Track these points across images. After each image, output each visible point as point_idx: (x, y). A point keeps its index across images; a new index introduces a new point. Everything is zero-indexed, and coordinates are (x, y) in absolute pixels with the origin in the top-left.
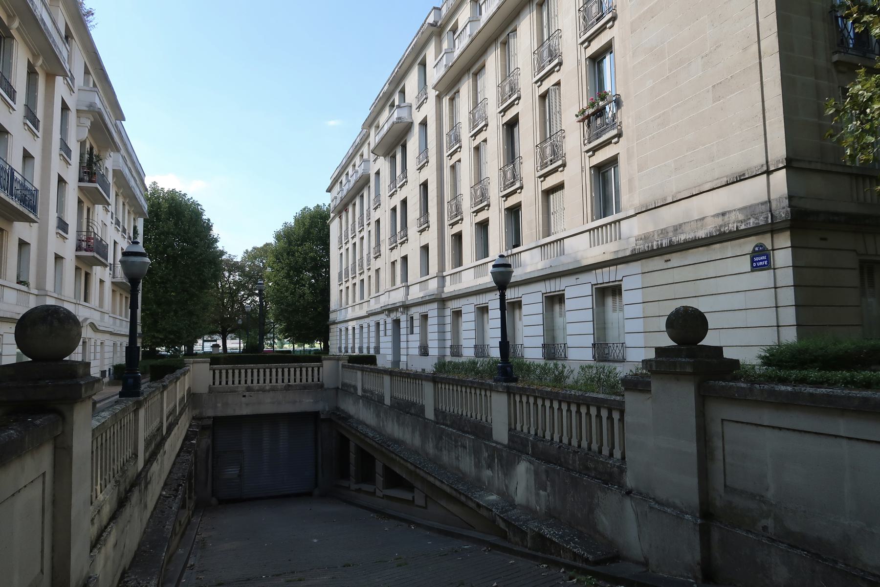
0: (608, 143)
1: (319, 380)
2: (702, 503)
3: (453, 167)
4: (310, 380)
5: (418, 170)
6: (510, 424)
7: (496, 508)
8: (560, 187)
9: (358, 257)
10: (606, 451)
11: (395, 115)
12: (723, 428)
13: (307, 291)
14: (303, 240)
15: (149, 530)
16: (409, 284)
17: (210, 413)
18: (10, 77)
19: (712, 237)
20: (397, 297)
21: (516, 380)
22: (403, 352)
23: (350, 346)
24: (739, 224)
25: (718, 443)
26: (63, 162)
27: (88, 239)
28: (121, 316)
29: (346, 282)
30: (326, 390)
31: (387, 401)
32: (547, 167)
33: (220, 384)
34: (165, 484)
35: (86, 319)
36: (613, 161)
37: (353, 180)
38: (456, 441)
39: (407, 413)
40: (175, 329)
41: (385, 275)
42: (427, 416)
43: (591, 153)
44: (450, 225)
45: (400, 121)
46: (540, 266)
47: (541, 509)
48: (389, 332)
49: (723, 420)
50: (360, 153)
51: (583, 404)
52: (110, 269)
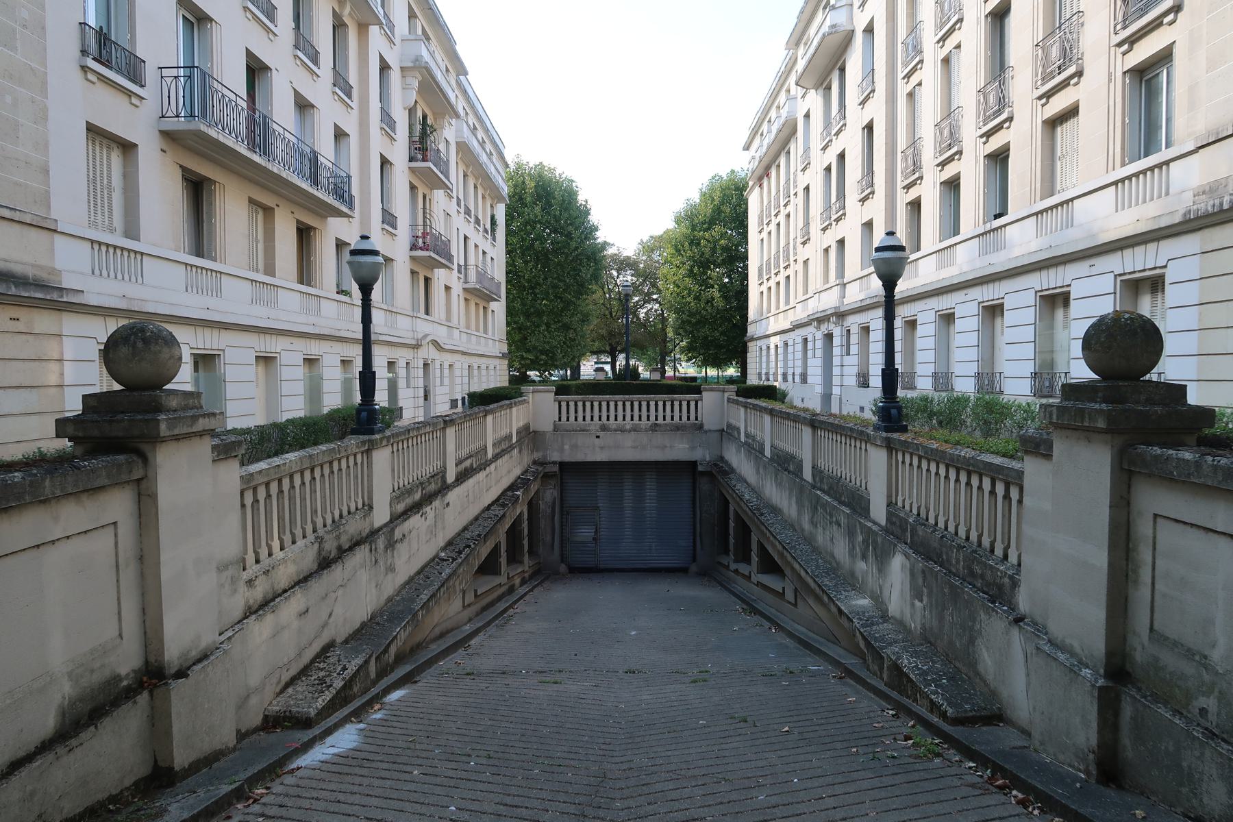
0: (1156, 24)
1: (697, 419)
2: (1110, 654)
3: (911, 95)
4: (684, 418)
5: (860, 104)
6: (889, 496)
7: (860, 619)
8: (1071, 112)
9: (782, 244)
10: (999, 552)
11: (828, 23)
12: (1155, 529)
13: (717, 295)
14: (711, 222)
15: (398, 598)
16: (846, 281)
17: (556, 457)
18: (311, 34)
20: (829, 301)
21: (904, 429)
22: (836, 381)
23: (772, 371)
25: (1145, 555)
26: (385, 137)
27: (425, 235)
28: (479, 332)
29: (768, 280)
30: (706, 432)
31: (768, 453)
32: (1053, 78)
33: (568, 420)
34: (450, 543)
35: (426, 336)
36: (1165, 57)
37: (775, 128)
38: (831, 516)
39: (785, 470)
40: (547, 347)
41: (816, 269)
42: (804, 477)
43: (1126, 47)
44: (904, 188)
45: (834, 30)
46: (1034, 246)
47: (915, 627)
48: (819, 353)
49: (1156, 516)
50: (785, 87)
51: (975, 472)
52: (459, 272)
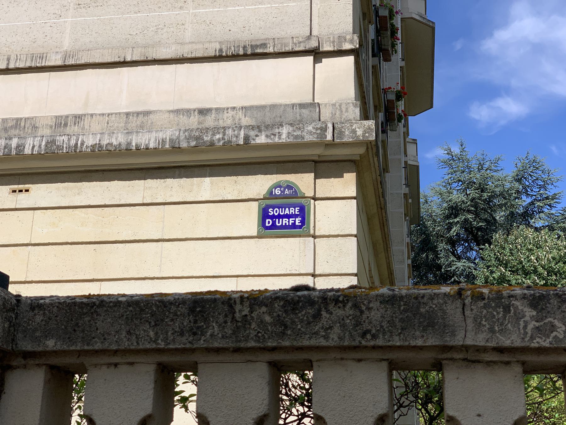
19: (176, 149)
24: (252, 133)
